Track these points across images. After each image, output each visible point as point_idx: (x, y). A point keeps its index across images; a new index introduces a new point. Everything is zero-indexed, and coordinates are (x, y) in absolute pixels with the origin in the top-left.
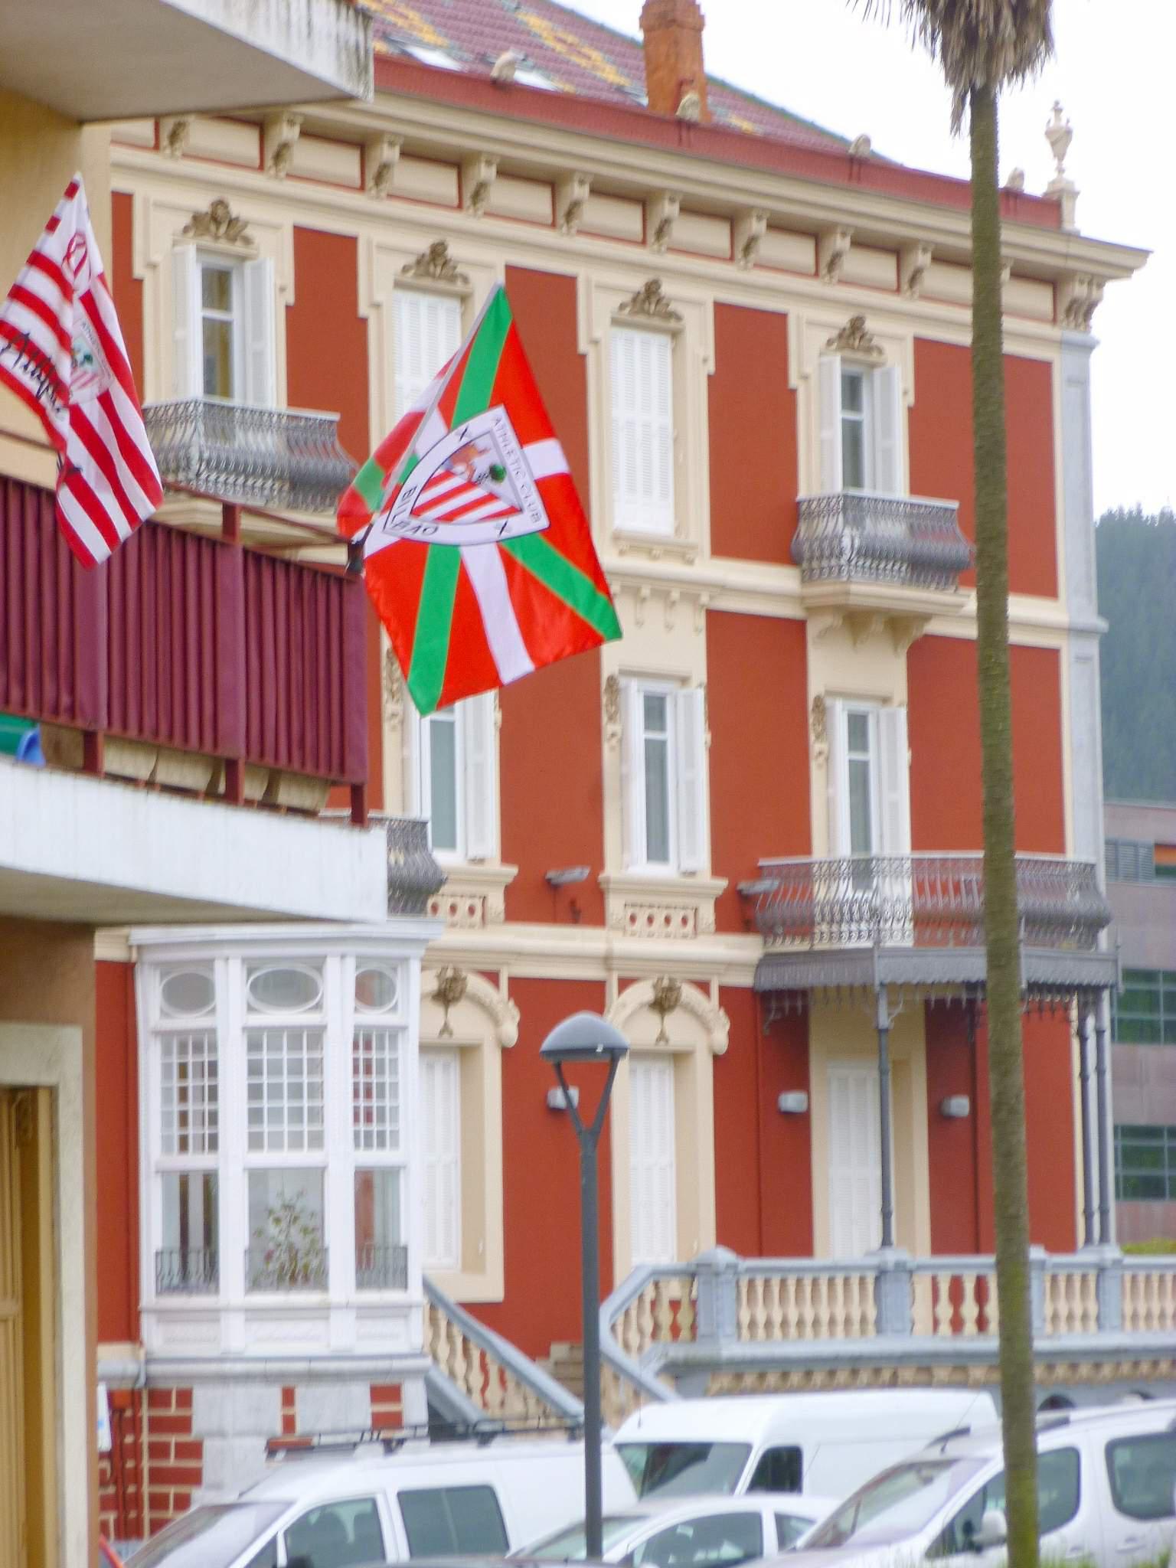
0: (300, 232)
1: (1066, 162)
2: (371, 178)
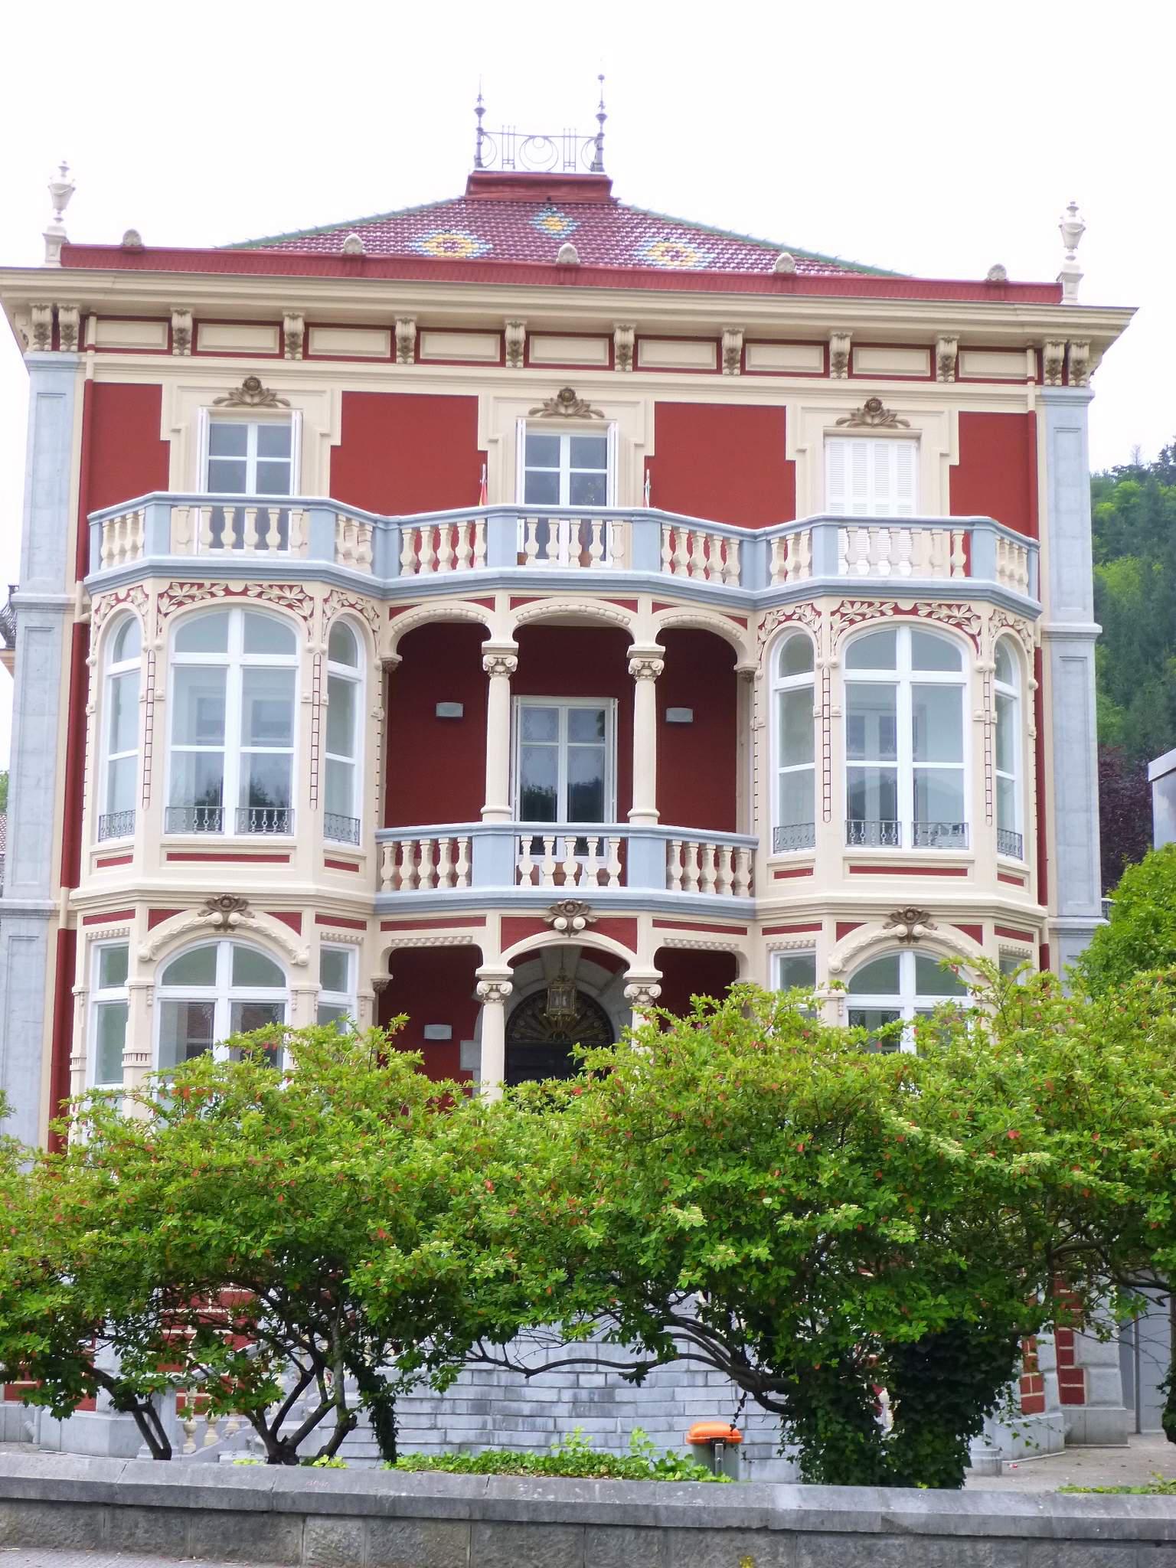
0: (964, 417)
1: (63, 214)
2: (176, 341)
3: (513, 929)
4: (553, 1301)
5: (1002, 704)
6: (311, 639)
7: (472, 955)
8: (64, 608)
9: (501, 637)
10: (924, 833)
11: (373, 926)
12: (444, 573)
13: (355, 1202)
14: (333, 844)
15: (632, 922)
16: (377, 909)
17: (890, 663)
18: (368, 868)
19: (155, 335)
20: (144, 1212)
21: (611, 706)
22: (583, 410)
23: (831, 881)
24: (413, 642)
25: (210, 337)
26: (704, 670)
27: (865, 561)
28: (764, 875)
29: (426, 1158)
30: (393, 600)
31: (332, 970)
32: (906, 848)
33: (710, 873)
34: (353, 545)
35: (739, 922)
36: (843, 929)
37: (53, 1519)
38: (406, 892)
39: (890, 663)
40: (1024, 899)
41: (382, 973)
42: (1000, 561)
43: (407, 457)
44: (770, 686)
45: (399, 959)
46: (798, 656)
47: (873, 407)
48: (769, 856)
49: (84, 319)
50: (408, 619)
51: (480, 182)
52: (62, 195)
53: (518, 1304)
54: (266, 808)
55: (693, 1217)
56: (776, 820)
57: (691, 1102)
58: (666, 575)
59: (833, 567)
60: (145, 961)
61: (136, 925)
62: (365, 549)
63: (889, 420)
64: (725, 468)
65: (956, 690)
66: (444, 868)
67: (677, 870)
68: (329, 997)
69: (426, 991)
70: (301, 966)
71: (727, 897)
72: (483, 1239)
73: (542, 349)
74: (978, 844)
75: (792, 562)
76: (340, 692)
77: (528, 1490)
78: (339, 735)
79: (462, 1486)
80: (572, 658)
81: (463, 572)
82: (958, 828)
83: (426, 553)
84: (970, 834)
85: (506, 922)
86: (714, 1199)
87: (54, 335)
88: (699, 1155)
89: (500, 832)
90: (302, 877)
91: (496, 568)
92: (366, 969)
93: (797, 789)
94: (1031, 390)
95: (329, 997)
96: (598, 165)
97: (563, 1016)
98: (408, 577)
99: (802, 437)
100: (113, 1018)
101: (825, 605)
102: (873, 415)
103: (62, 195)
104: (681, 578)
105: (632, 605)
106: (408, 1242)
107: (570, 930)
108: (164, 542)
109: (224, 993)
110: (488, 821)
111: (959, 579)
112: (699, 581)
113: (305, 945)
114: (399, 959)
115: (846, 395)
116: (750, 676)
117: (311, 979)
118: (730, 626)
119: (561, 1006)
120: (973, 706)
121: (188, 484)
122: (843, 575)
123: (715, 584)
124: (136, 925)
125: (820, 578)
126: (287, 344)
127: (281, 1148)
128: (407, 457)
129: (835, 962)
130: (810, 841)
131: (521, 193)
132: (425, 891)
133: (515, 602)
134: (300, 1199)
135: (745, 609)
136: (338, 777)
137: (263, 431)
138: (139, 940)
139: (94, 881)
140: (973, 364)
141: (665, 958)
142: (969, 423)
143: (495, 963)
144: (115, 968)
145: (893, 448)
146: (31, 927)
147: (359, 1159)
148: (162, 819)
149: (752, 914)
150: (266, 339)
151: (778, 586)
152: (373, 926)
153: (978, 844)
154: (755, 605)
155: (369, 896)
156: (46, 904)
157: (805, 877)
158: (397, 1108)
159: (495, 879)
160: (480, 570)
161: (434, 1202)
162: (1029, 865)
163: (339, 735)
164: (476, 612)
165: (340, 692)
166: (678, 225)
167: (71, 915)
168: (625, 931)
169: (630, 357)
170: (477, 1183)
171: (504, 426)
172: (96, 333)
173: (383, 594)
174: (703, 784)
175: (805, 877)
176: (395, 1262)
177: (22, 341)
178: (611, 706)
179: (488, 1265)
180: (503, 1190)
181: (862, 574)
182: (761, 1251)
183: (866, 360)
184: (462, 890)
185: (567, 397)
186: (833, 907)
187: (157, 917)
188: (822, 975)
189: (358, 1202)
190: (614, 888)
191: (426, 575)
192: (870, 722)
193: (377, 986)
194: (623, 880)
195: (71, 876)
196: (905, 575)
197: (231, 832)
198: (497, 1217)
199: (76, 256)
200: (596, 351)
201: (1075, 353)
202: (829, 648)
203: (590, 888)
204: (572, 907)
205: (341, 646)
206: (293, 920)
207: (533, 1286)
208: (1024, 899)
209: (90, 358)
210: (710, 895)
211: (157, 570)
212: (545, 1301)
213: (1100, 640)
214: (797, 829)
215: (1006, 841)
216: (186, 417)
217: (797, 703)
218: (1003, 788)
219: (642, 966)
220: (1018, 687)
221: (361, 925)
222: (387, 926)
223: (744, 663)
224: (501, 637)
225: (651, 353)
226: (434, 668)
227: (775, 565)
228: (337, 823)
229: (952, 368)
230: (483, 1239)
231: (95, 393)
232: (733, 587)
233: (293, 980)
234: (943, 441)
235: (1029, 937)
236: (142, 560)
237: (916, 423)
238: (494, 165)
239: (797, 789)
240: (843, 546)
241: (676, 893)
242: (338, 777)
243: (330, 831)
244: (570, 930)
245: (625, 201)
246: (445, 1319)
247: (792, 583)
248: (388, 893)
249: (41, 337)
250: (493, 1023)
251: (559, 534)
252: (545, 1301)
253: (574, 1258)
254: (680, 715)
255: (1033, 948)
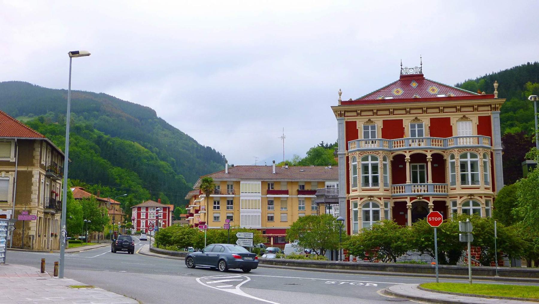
2: (358, 114)
3: (411, 199)
4: (411, 248)
5: (485, 163)
6: (380, 159)
7: (406, 203)
8: (345, 154)
9: (408, 157)
10: (473, 183)
11: (392, 198)
12: (399, 148)
13: (391, 238)
14: (385, 187)
15: (429, 198)
16: (392, 196)
17: (467, 158)
18: (390, 191)
19: (355, 114)
20: (370, 240)
21: (425, 164)
22: (419, 120)
23: (459, 191)
24: (394, 157)
25: (363, 113)
26: (439, 161)
27: (462, 143)
28: (449, 190)
29: (398, 234)
30: (392, 152)
31: (386, 205)
32: (470, 185)
33: (441, 190)
34: (386, 145)
35: (446, 196)
36: (461, 197)
37: (365, 268)
38: (396, 194)
39: (467, 158)
40: (490, 192)
41: (393, 205)
42: (485, 142)
43: (393, 130)
44: (449, 161)
45: (395, 203)
46: (453, 157)
47: (464, 116)
48: (450, 187)
49: (345, 112)
50: (394, 154)
51: (402, 77)
52: (340, 94)
53: (407, 248)
54: (375, 180)
55: (423, 240)
56: (451, 181)
57: (423, 229)
58: (432, 146)
59: (457, 144)
60: (360, 205)
61: (358, 200)
62: (387, 145)
63: (467, 118)
64: (441, 128)
65: (477, 161)
66: (401, 190)
67: (435, 189)
68: (386, 209)
69: (399, 209)
70: (382, 205)
71: (443, 193)
72: (404, 242)
73: (412, 111)
74: (481, 183)
75: (451, 143)
76: (385, 165)
77: (408, 265)
78: (385, 172)
79: (402, 264)
80: (418, 158)
81: (402, 148)
82: (478, 181)
83: (396, 145)
84: (480, 183)
85: (410, 198)
86: (426, 238)
87: (341, 115)
88: (424, 234)
89: (409, 185)
90: (380, 193)
91: (407, 146)
92: (391, 205)
93: (453, 177)
94: (490, 112)
95: (386, 209)
96: (421, 72)
97: (420, 211)
98: (394, 148)
99: (453, 122)
100: (356, 213)
101: (456, 150)
102: (464, 118)
103: (340, 94)
104: (434, 147)
105: (427, 151)
106: (396, 242)
107: (420, 199)
108: (359, 146)
109: (371, 209)
110: (407, 184)
111: (477, 145)
112: (437, 147)
113: (382, 202)
114: (395, 203)
115: (460, 115)
116: (446, 160)
117: (383, 207)
118: (442, 153)
119: (420, 209)
120: (480, 164)
121: (361, 137)
122: (459, 145)
123: (440, 147)
124: (358, 200)
125: (455, 146)
126: (374, 114)
127: (383, 233)
128: (393, 130)
129: (460, 202)
130: (455, 185)
131: (409, 78)
132: (399, 194)
133: (409, 152)
134: (386, 238)
135: (445, 150)
136: (385, 178)
137: (371, 126)
138: (359, 202)
139: (352, 194)
140: (480, 109)
141: (434, 202)
142: (480, 118)
143: (409, 204)
144: (356, 206)
145: (468, 123)
146: (343, 200)
147: (390, 234)
148: (361, 185)
149: (447, 195)
150: (371, 113)
151: (449, 147)
152: (392, 198)
153: (481, 183)
154: (446, 149)
155: (391, 194)
156: (345, 196)
157: (456, 190)
158: (395, 228)
159: (410, 191)
160: (404, 147)
161: (399, 238)
162: (490, 186)
163: (385, 172)
164: (404, 153)
165: (385, 165)
166: (434, 83)
167: (349, 198)
168: (428, 199)
169: (426, 112)
170: (403, 237)
171: (407, 124)
172: (347, 114)
173: (390, 151)
174: (439, 176)
175: (456, 190)
176: (395, 244)
177: (336, 116)
178: (425, 164)
179: (404, 245)
180: (406, 237)
181: (461, 145)
182: (430, 243)
183: (463, 109)
184: (404, 193)
185: (416, 118)
186: (459, 194)
187: (361, 199)
188: (458, 204)
189: (391, 238)
190: (426, 193)
191: (396, 148)
192: (463, 166)
193: (393, 207)
194: (427, 191)
195: (348, 192)
196: (468, 145)
197: (370, 187)
198: (405, 240)
199: (343, 103)
200: (420, 111)
201: (497, 106)
202: (457, 156)
203: (423, 193)
204: (420, 196)
205: (385, 159)
206: (380, 199)
207: (409, 247)
208: (490, 192)
209: (346, 118)
210: (441, 193)
211: (358, 150)
212: (410, 248)
213: (503, 151)
214: (453, 183)
215: (486, 183)
216: (360, 126)
217: (453, 164)
218: (486, 175)
219: (431, 204)
220: (488, 160)
221: (389, 199)
222: (393, 199)
223: (445, 158)
224: (408, 157)
225: (429, 111)
226: (398, 161)
227: (449, 143)
228: (386, 184)
229: (477, 110)
230: (404, 242)
231: (347, 123)
232: (442, 147)
233: (381, 207)
234: (476, 121)
235: (491, 197)
236: (356, 149)
237: (471, 118)
238: (404, 73)
239: (453, 177)
240: (459, 141)
241: (436, 193)
242: (385, 178)
243: (384, 186)
244: (420, 199)
245: (426, 78)
246: (401, 250)
247: (451, 146)
248: (393, 194)
249: (339, 115)
250: (409, 212)
251: (417, 141)
252: (410, 248)
253: (413, 244)
254: (435, 165)
255: (492, 199)
